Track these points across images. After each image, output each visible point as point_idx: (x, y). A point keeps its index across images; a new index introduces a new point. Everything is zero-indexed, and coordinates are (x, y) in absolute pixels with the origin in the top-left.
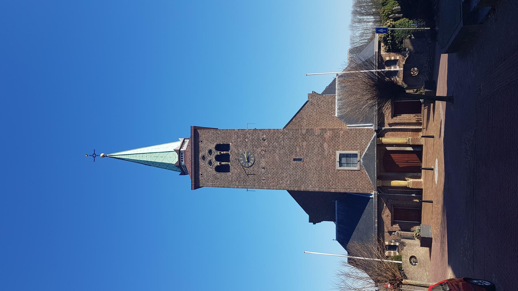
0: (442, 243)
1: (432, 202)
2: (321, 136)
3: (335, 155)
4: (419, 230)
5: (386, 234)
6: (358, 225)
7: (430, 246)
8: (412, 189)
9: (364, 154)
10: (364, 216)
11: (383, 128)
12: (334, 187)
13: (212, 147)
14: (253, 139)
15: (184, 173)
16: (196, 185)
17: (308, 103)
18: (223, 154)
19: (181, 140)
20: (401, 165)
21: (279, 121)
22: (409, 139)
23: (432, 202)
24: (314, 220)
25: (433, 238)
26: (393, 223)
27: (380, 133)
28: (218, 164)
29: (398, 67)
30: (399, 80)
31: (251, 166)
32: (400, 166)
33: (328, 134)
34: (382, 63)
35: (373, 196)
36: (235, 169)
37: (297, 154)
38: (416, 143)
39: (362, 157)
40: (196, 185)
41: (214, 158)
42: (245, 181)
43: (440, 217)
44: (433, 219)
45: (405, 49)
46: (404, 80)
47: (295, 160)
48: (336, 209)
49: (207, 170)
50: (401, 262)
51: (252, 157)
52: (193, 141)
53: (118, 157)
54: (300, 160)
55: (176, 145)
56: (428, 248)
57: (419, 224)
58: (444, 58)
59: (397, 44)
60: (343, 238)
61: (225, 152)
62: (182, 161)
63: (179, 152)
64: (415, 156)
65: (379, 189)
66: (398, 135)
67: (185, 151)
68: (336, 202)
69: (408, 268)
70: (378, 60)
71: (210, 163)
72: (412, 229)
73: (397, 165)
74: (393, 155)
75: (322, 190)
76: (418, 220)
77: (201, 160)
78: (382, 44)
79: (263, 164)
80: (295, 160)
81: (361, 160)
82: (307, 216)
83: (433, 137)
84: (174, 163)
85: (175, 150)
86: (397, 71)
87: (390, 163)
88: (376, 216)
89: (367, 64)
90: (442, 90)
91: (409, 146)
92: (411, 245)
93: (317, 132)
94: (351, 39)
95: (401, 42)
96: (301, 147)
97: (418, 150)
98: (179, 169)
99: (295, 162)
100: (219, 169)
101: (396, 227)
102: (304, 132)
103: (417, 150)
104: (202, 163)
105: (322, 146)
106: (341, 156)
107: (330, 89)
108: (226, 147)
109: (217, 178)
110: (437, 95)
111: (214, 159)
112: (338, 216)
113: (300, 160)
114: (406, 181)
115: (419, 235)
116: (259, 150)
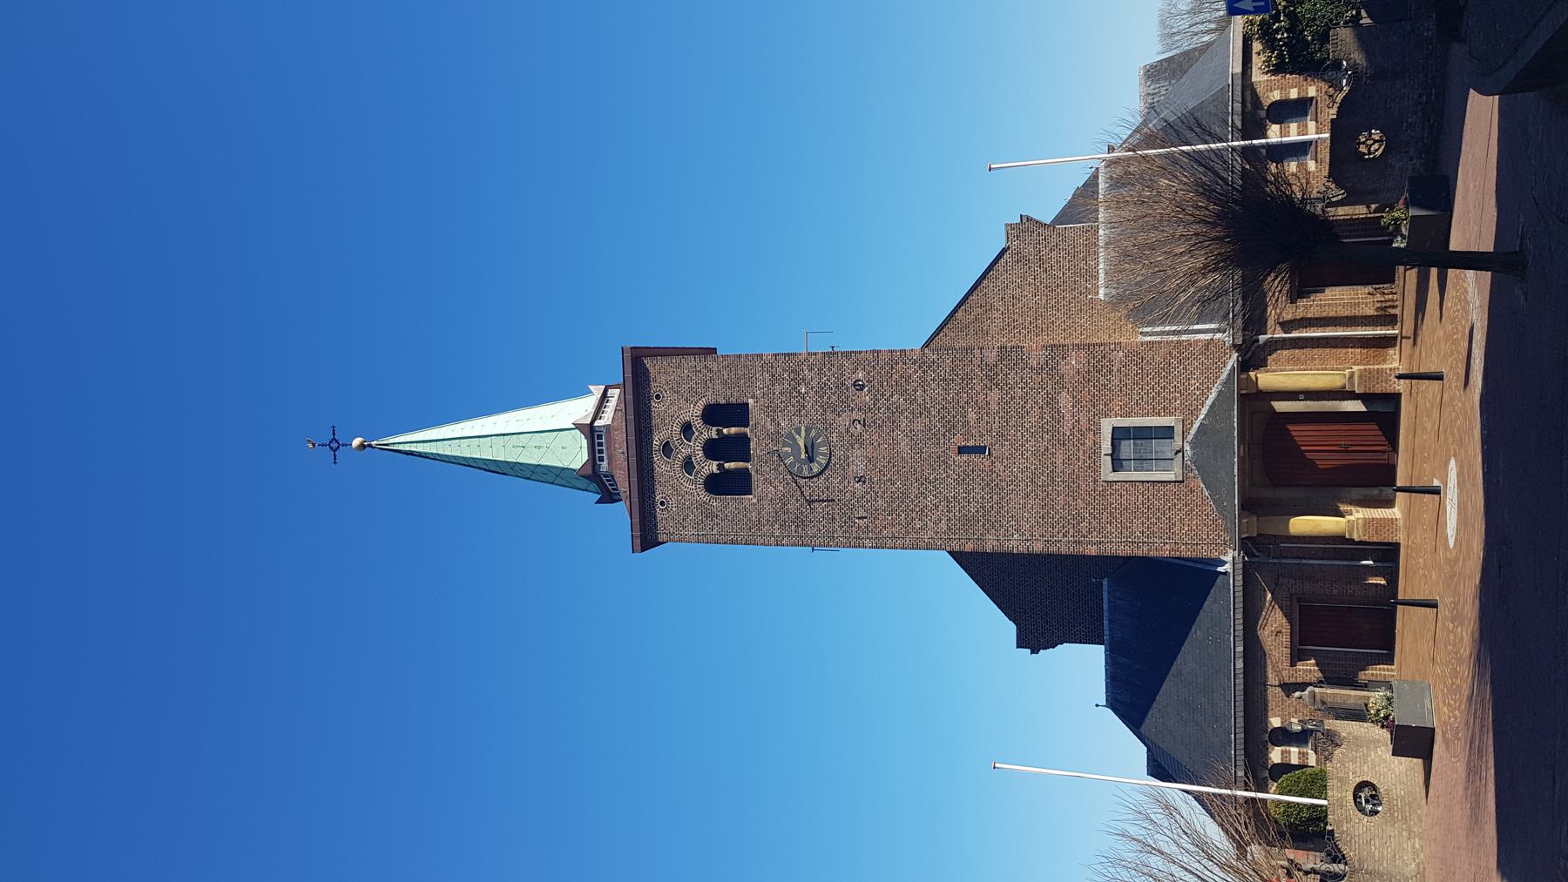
0: (1475, 752)
1: (1433, 605)
2: (1049, 368)
3: (1097, 432)
5: (1274, 694)
7: (1427, 757)
9: (1196, 426)
10: (1197, 633)
11: (1262, 338)
13: (693, 412)
14: (822, 387)
15: (609, 496)
16: (647, 537)
17: (1006, 256)
18: (729, 437)
19: (597, 391)
21: (907, 326)
23: (1433, 605)
24: (1034, 638)
26: (1297, 656)
27: (1252, 356)
28: (715, 470)
29: (1312, 125)
30: (1310, 175)
31: (821, 473)
32: (1321, 465)
33: (1073, 363)
34: (1255, 116)
36: (767, 486)
37: (968, 432)
38: (1378, 389)
39: (1190, 438)
40: (647, 537)
41: (703, 450)
42: (800, 523)
43: (1466, 671)
44: (1435, 661)
45: (1337, 65)
46: (1336, 174)
47: (962, 450)
48: (1105, 606)
49: (679, 489)
50: (1324, 802)
51: (821, 445)
52: (630, 397)
53: (407, 448)
54: (979, 450)
55: (580, 408)
56: (1419, 761)
57: (1389, 659)
58: (1482, 115)
59: (1308, 44)
60: (1131, 697)
61: (733, 430)
62: (601, 459)
63: (590, 431)
64: (1372, 431)
65: (1248, 545)
66: (1313, 359)
67: (607, 427)
68: (1105, 582)
69: (1347, 822)
70: (1243, 103)
71: (688, 465)
72: (1364, 676)
75: (1053, 549)
76: (1384, 645)
77: (658, 459)
78: (1257, 46)
79: (859, 467)
80: (962, 450)
81: (1187, 447)
82: (1010, 629)
83: (1438, 377)
84: (577, 465)
85: (578, 426)
86: (1310, 142)
87: (1283, 456)
88: (1240, 633)
89: (1193, 126)
90: (1473, 221)
91: (1352, 396)
92: (1358, 742)
94: (1162, 22)
95: (1324, 38)
96: (983, 408)
97: (1383, 412)
98: (593, 486)
99: (965, 457)
100: (716, 485)
101: (1308, 669)
102: (991, 356)
103: (1379, 408)
104: (661, 466)
105: (1052, 401)
106: (1119, 435)
107: (1080, 206)
108: (735, 413)
109: (711, 515)
110: (1453, 246)
111: (701, 454)
112: (1111, 630)
113: (979, 450)
114: (1342, 516)
115: (1386, 718)
116: (844, 420)
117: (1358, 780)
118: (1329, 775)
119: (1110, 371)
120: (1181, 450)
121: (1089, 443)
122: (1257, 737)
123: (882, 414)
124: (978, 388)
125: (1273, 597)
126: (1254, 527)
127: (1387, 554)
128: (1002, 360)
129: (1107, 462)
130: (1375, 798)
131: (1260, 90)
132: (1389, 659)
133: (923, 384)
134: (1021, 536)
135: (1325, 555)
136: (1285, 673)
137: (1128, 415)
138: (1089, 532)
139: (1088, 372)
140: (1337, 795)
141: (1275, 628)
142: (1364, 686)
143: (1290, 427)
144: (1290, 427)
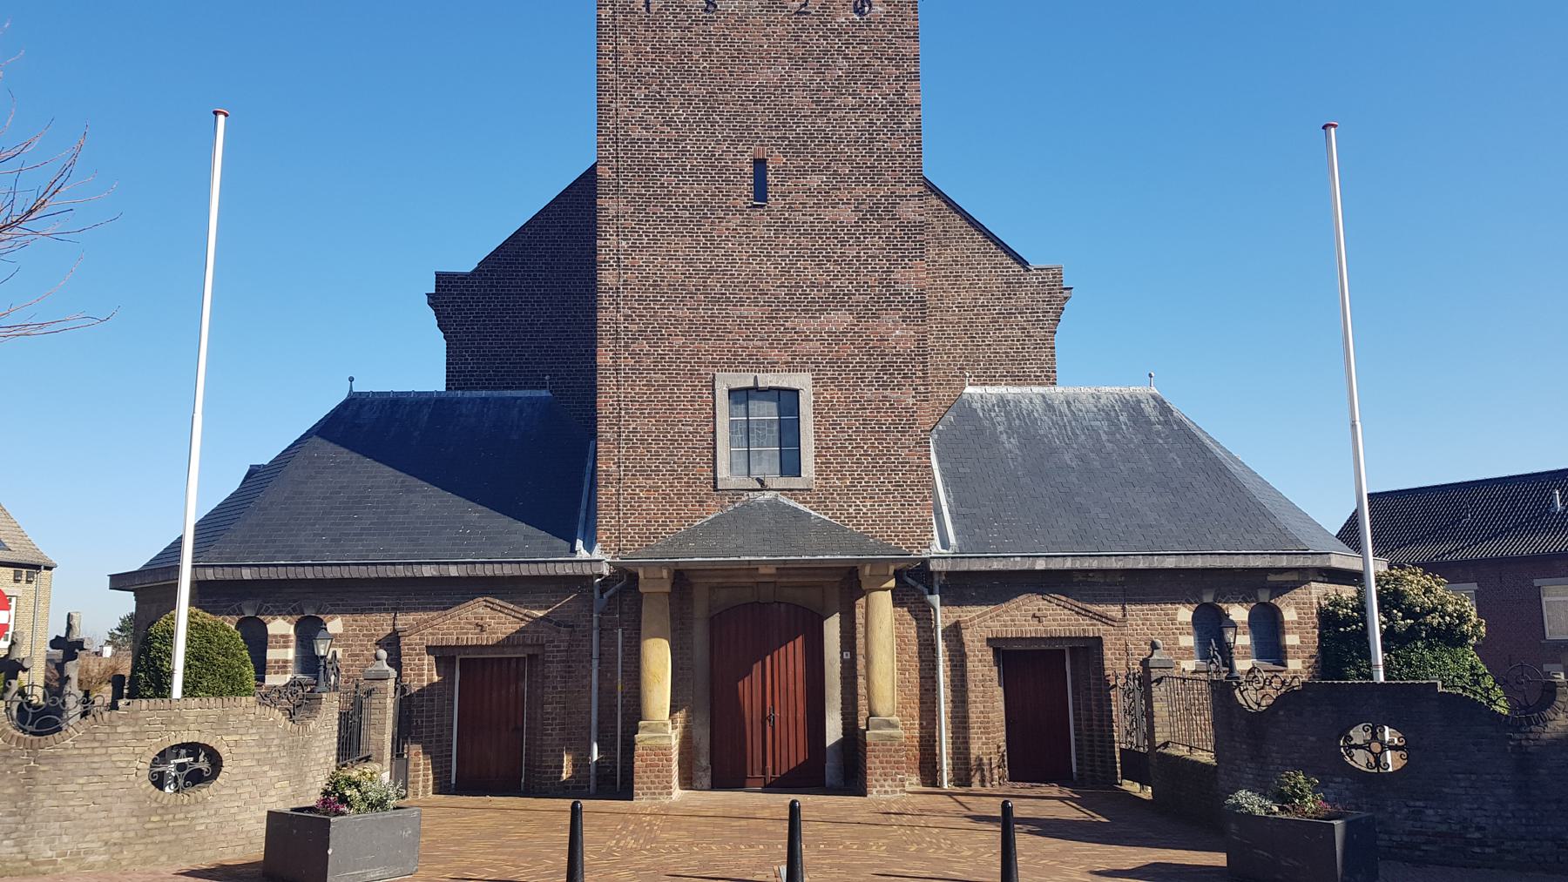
2: (889, 296)
3: (791, 367)
4: (381, 804)
5: (382, 623)
6: (427, 487)
8: (629, 746)
10: (475, 513)
11: (936, 599)
12: (626, 362)
17: (1017, 267)
20: (749, 690)
22: (891, 725)
24: (452, 298)
26: (444, 655)
27: (914, 582)
32: (744, 686)
33: (898, 332)
35: (583, 554)
38: (873, 764)
39: (783, 499)
47: (760, 165)
48: (508, 393)
54: (761, 191)
57: (442, 787)
58: (1219, 859)
60: (363, 425)
64: (794, 753)
65: (625, 580)
68: (544, 393)
72: (415, 752)
73: (750, 672)
74: (795, 649)
75: (604, 300)
76: (465, 779)
80: (760, 165)
82: (467, 264)
92: (298, 750)
93: (910, 278)
96: (826, 197)
99: (749, 169)
101: (423, 673)
103: (831, 768)
105: (837, 300)
106: (787, 399)
112: (472, 400)
113: (761, 191)
115: (343, 800)
117: (223, 751)
118: (230, 701)
119: (884, 386)
120: (763, 487)
121: (774, 354)
122: (310, 600)
123: (817, 42)
124: (859, 191)
125: (537, 620)
126: (655, 586)
127: (616, 781)
128: (902, 227)
129: (745, 380)
130: (196, 778)
131: (1299, 593)
132: (442, 787)
133: (864, 107)
134: (623, 258)
135: (607, 694)
136: (415, 638)
137: (817, 411)
138: (633, 354)
139: (883, 355)
140: (191, 716)
141: (488, 623)
142: (398, 753)
143: (799, 641)
144: (799, 641)
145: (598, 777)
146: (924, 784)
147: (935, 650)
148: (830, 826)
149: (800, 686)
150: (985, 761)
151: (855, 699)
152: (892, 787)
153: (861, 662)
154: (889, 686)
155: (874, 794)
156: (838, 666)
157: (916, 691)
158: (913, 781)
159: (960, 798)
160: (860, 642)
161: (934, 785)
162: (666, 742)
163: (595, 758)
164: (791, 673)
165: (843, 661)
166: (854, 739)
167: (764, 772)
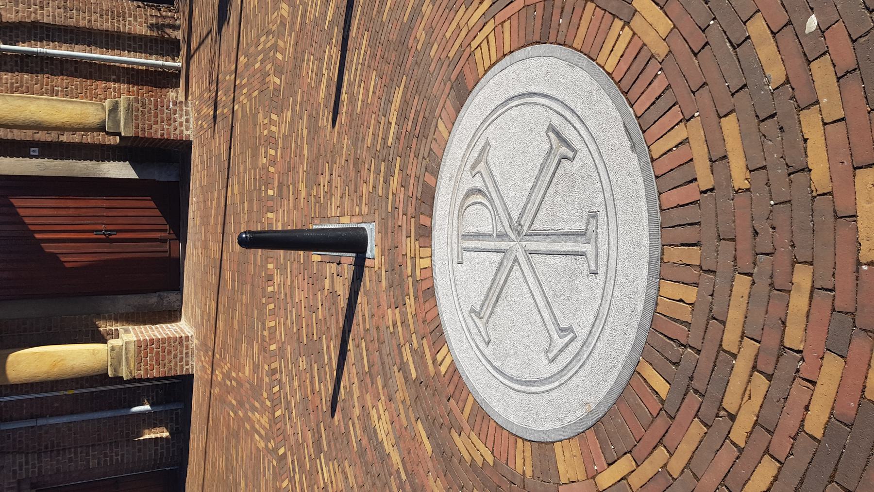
20: (73, 257)
22: (114, 109)
25: (194, 142)
38: (158, 131)
64: (146, 210)
73: (54, 256)
103: (159, 175)
114: (105, 342)
127: (172, 394)
135: (77, 405)
143: (16, 202)
144: (16, 202)
145: (168, 402)
146: (177, 85)
147: (28, 55)
148: (234, 180)
149: (70, 203)
150: (154, 21)
151: (87, 145)
152: (185, 116)
153: (42, 136)
154: (69, 107)
155: (189, 133)
156: (46, 162)
157: (77, 81)
158: (174, 95)
159: (194, 45)
160: (17, 135)
161: (178, 76)
162: (132, 347)
163: (147, 407)
164: (55, 212)
165: (41, 156)
166: (130, 150)
167: (164, 241)
